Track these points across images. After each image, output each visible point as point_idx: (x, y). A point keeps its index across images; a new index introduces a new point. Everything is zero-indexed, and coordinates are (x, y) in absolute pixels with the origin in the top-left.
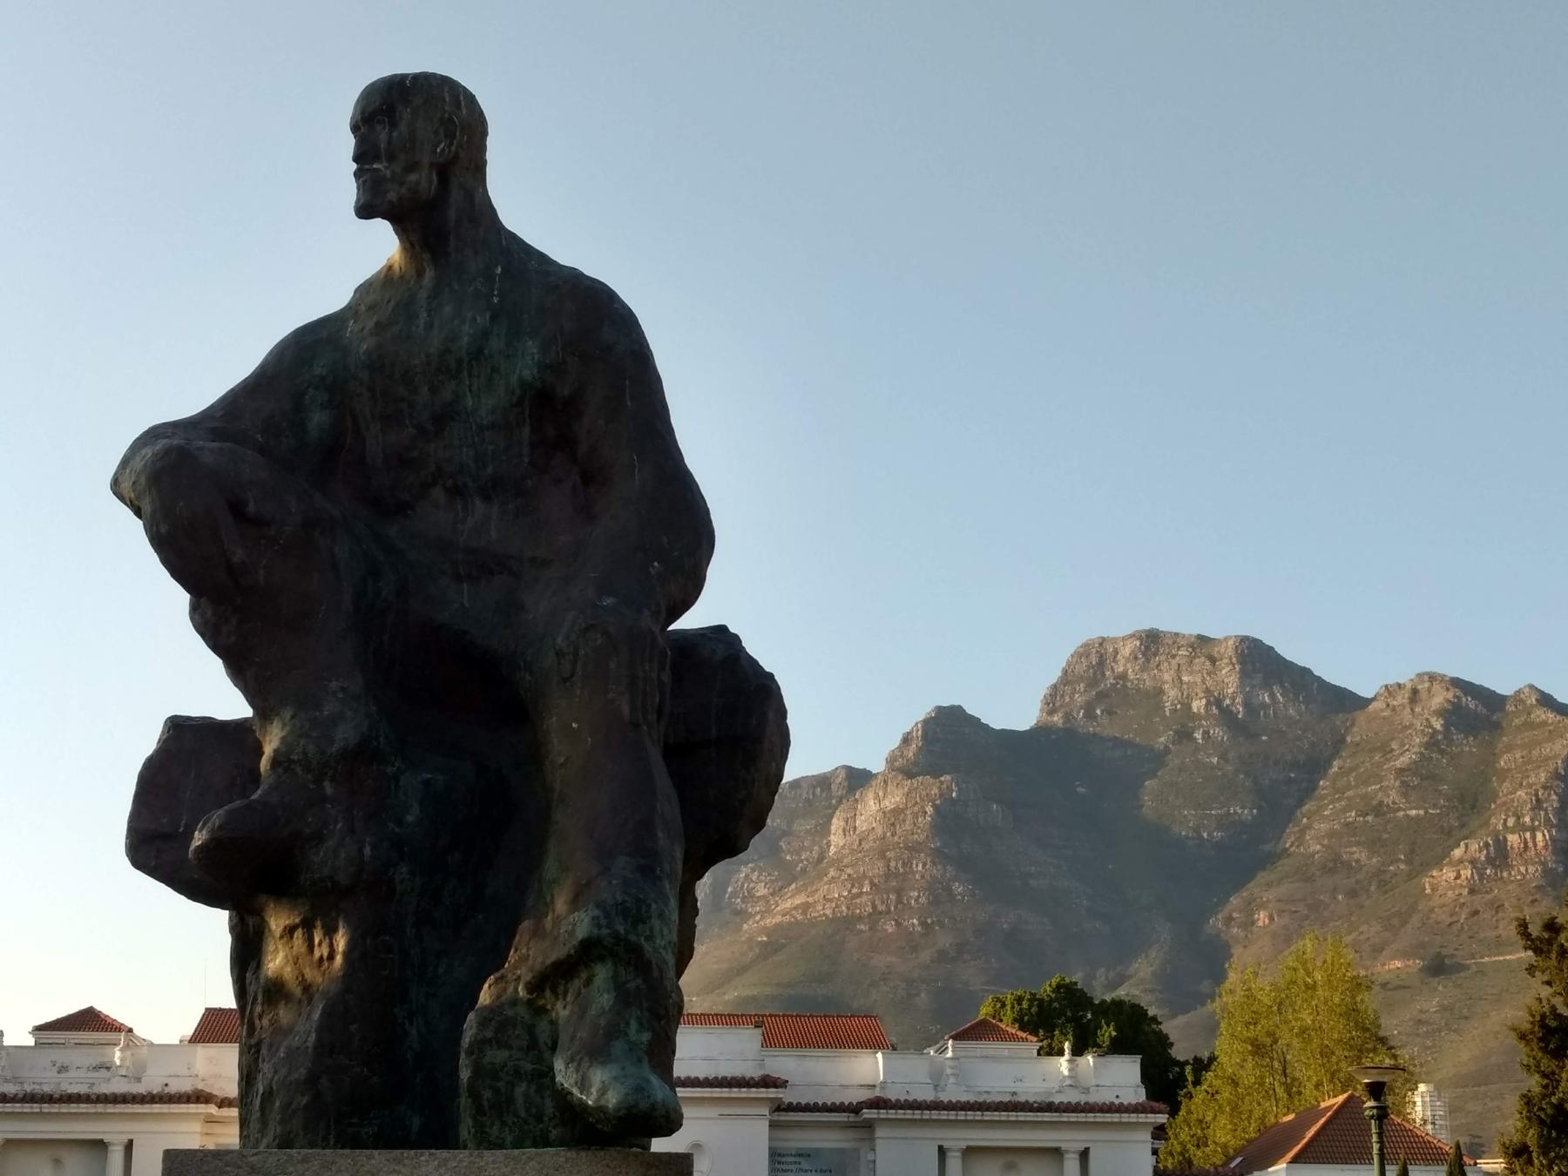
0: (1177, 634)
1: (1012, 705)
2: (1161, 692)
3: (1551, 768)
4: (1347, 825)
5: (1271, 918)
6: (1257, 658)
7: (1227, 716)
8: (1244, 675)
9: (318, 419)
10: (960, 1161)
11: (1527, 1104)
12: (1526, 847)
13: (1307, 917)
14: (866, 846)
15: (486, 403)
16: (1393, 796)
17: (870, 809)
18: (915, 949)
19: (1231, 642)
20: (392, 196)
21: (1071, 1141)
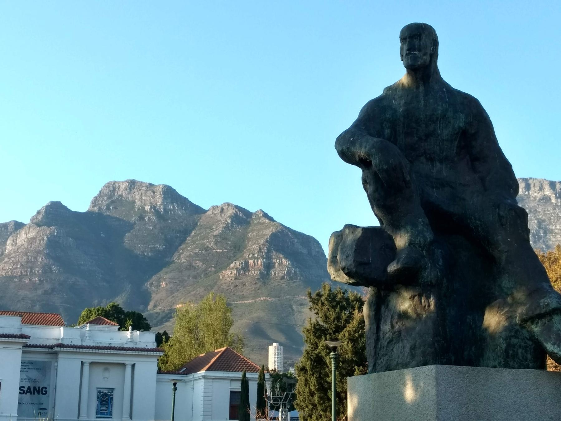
1: (80, 203)
2: (134, 202)
4: (196, 253)
5: (166, 284)
6: (170, 193)
7: (157, 212)
8: (165, 198)
12: (255, 265)
13: (179, 285)
14: (20, 250)
15: (445, 133)
16: (212, 245)
17: (23, 237)
18: (36, 289)
19: (161, 187)
21: (129, 361)
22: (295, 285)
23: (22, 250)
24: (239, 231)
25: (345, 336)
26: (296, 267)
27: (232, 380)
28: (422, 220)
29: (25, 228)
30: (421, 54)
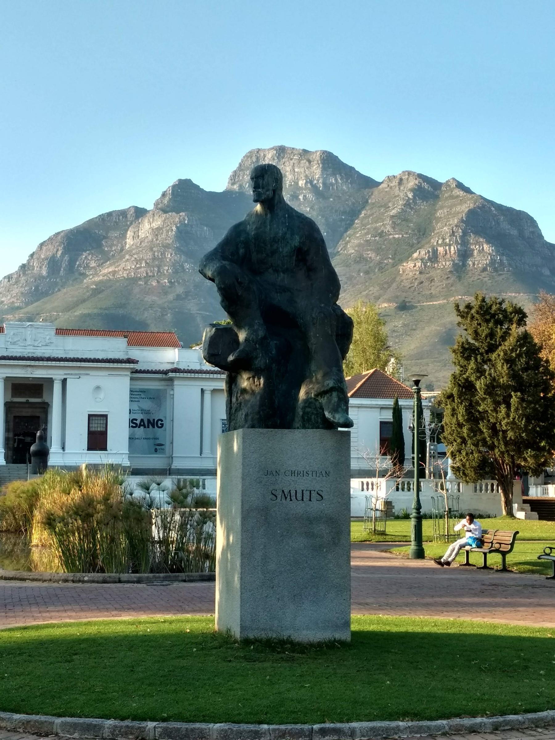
0: (293, 148)
3: (460, 217)
4: (367, 241)
7: (315, 188)
8: (324, 169)
9: (241, 251)
10: (210, 395)
11: (454, 378)
13: (346, 283)
15: (285, 250)
16: (388, 228)
17: (146, 227)
19: (318, 153)
20: (263, 198)
22: (500, 278)
23: (146, 244)
24: (424, 209)
25: (499, 355)
26: (503, 254)
27: (382, 408)
28: (258, 321)
29: (148, 215)
30: (264, 190)
